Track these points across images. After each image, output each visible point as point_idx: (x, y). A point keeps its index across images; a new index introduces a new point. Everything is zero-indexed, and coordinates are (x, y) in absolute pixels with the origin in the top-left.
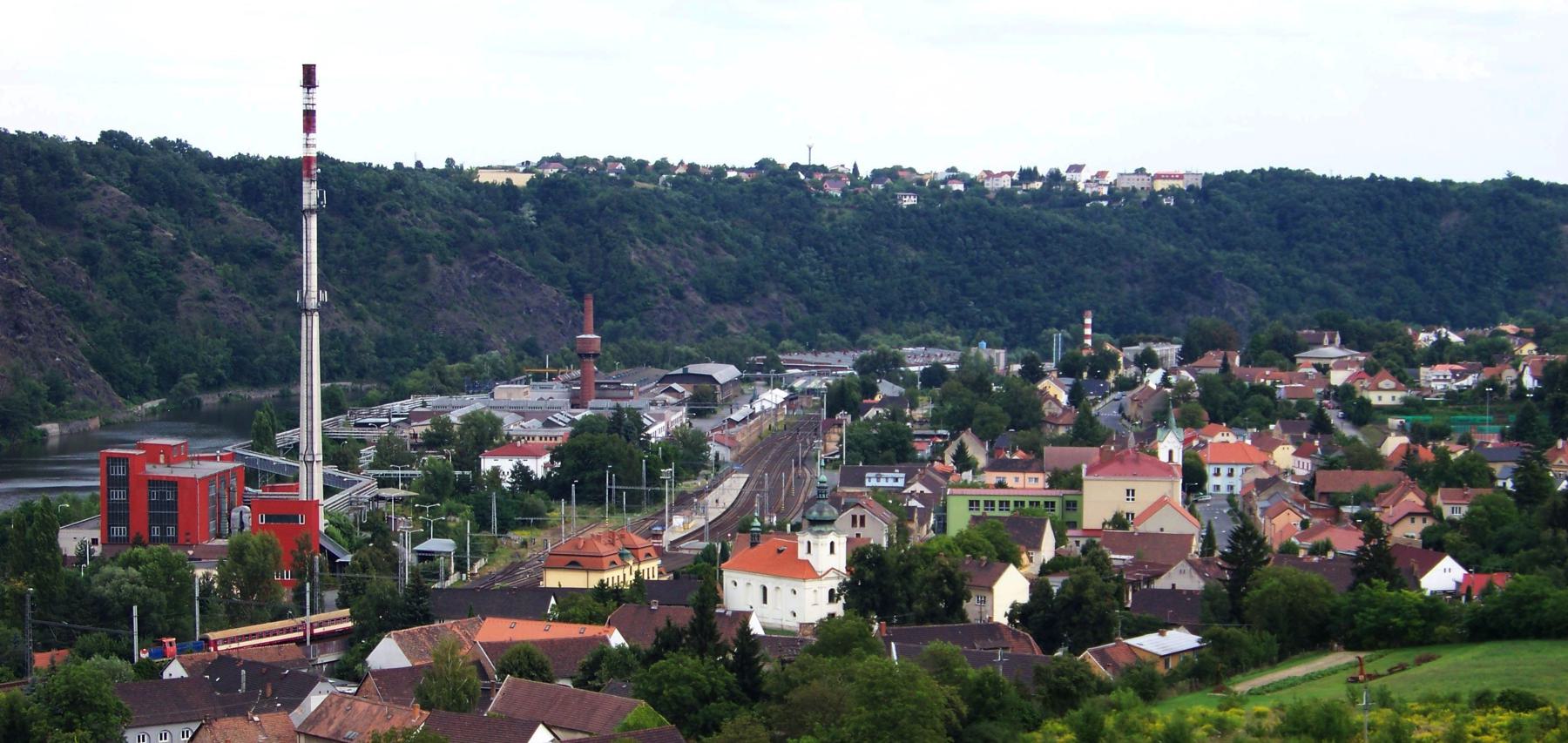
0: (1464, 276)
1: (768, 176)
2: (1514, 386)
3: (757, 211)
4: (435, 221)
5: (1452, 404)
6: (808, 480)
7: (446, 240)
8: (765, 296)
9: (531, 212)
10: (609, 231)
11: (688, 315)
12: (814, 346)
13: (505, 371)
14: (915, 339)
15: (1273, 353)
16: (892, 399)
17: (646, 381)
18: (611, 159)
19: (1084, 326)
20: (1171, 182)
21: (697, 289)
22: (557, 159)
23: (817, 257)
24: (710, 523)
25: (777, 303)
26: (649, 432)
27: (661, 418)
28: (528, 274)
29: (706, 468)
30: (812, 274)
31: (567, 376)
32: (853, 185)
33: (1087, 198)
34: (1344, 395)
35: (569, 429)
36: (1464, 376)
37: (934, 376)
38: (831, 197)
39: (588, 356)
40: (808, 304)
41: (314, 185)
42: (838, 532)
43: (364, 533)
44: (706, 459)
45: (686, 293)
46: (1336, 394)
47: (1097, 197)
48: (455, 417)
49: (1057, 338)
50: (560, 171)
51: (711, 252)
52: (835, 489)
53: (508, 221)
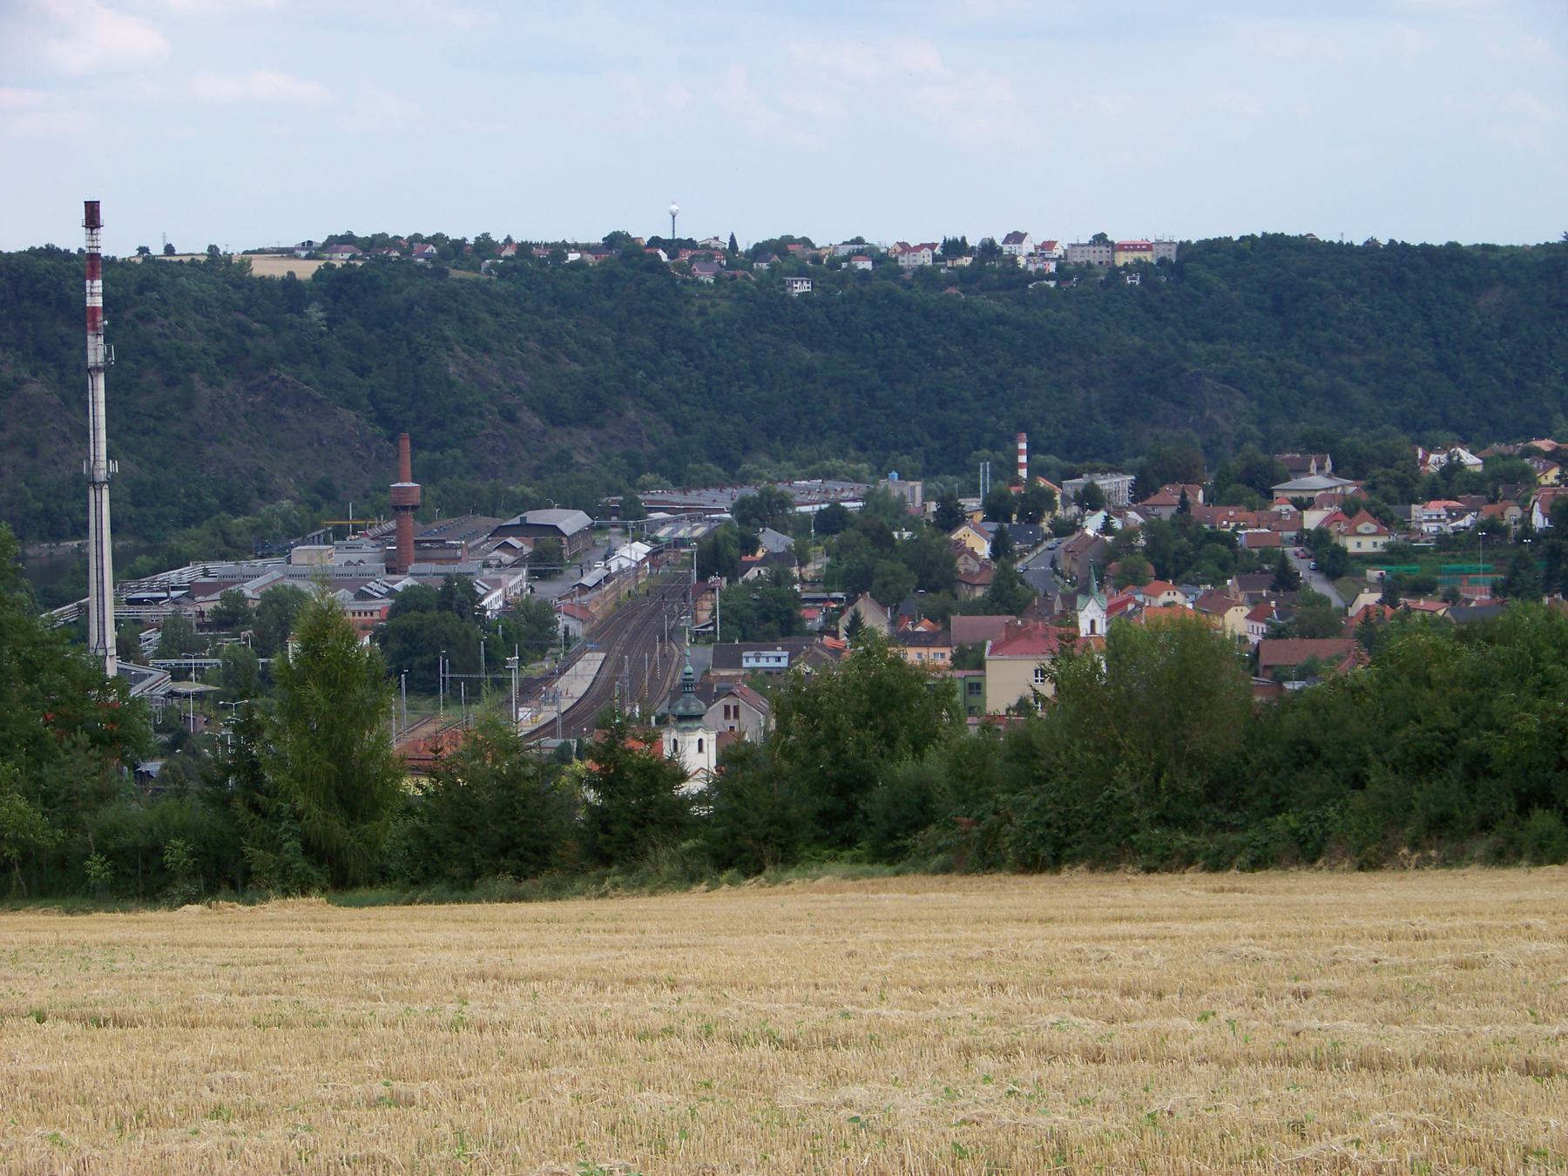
0: (1509, 370)
1: (620, 258)
2: (1519, 527)
3: (607, 304)
4: (201, 331)
5: (1444, 550)
6: (676, 659)
7: (215, 355)
8: (620, 415)
9: (321, 315)
10: (420, 338)
11: (523, 443)
12: (680, 481)
13: (299, 525)
14: (811, 468)
15: (1242, 488)
16: (777, 555)
17: (476, 534)
18: (417, 238)
19: (1018, 452)
20: (1136, 255)
21: (534, 409)
22: (348, 239)
23: (685, 364)
24: (563, 714)
25: (636, 423)
26: (484, 603)
27: (496, 584)
28: (320, 396)
29: (554, 646)
30: (679, 385)
31: (377, 531)
32: (730, 266)
33: (1026, 276)
34: (1317, 542)
35: (389, 602)
36: (1461, 516)
37: (832, 520)
38: (701, 284)
39: (405, 508)
40: (675, 424)
41: (101, 340)
42: (707, 729)
43: (159, 736)
44: (554, 635)
45: (519, 414)
46: (1308, 540)
47: (1042, 275)
48: (249, 590)
49: (985, 467)
50: (352, 258)
51: (548, 359)
52: (707, 672)
53: (291, 326)
